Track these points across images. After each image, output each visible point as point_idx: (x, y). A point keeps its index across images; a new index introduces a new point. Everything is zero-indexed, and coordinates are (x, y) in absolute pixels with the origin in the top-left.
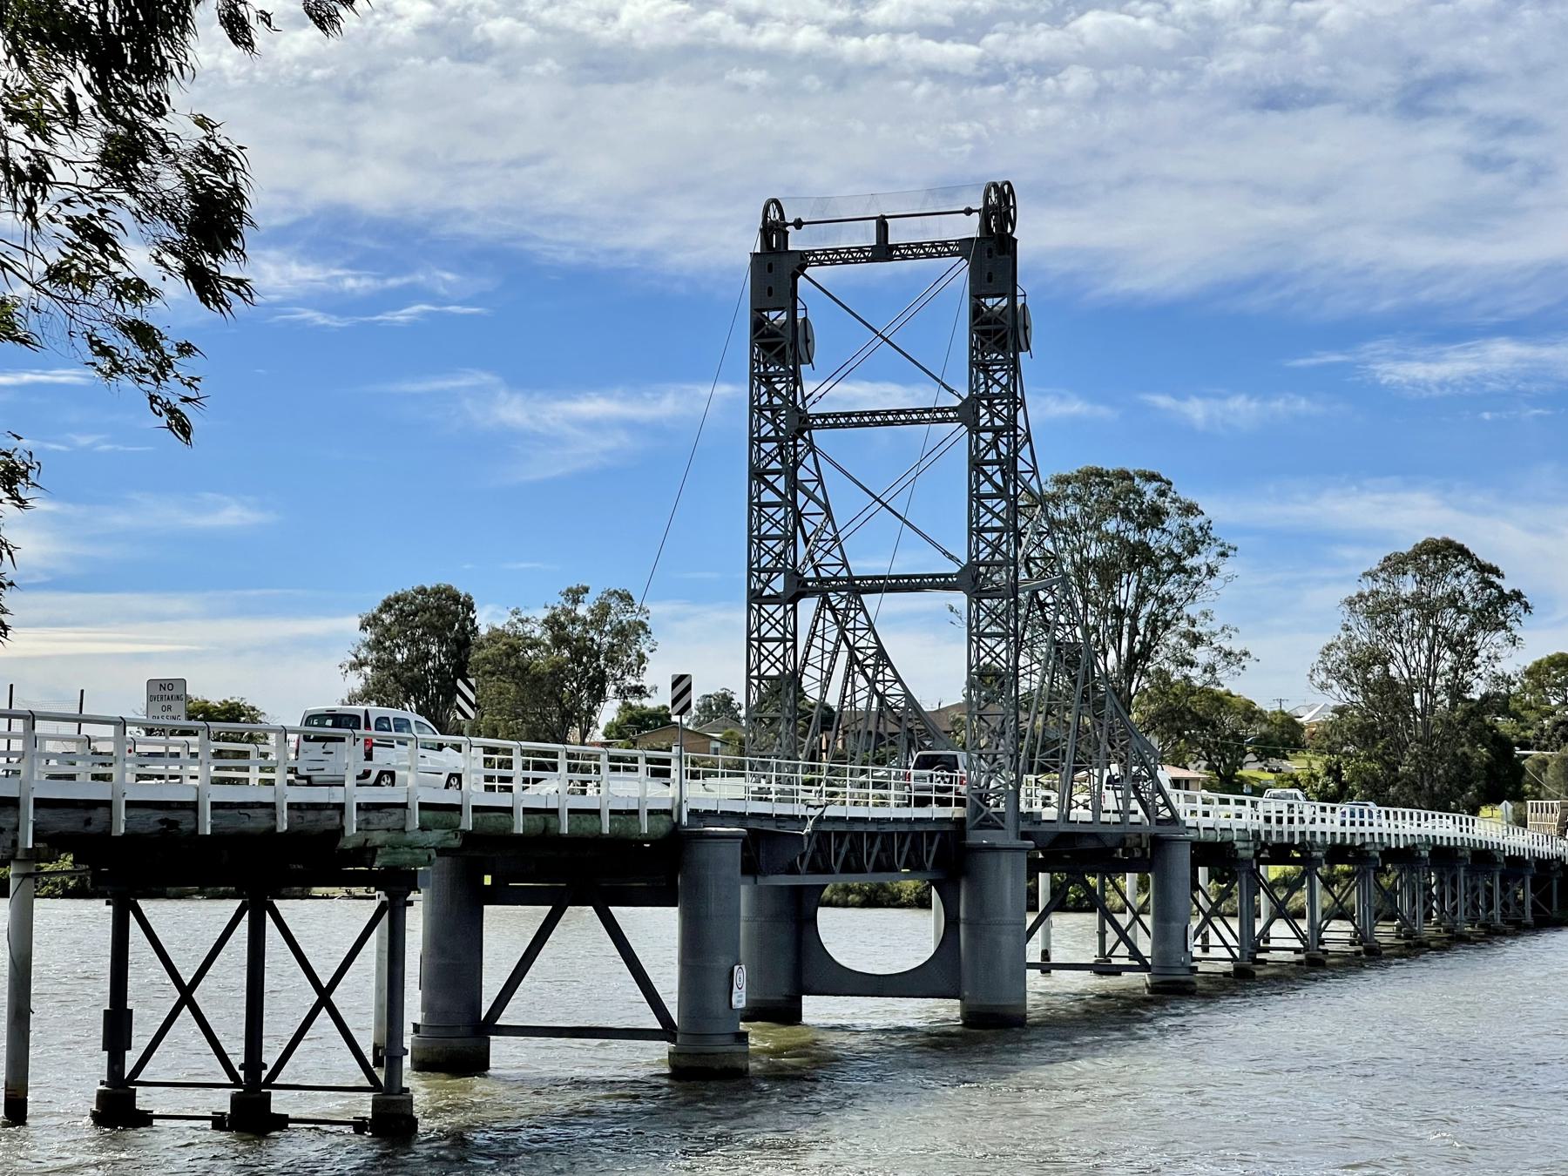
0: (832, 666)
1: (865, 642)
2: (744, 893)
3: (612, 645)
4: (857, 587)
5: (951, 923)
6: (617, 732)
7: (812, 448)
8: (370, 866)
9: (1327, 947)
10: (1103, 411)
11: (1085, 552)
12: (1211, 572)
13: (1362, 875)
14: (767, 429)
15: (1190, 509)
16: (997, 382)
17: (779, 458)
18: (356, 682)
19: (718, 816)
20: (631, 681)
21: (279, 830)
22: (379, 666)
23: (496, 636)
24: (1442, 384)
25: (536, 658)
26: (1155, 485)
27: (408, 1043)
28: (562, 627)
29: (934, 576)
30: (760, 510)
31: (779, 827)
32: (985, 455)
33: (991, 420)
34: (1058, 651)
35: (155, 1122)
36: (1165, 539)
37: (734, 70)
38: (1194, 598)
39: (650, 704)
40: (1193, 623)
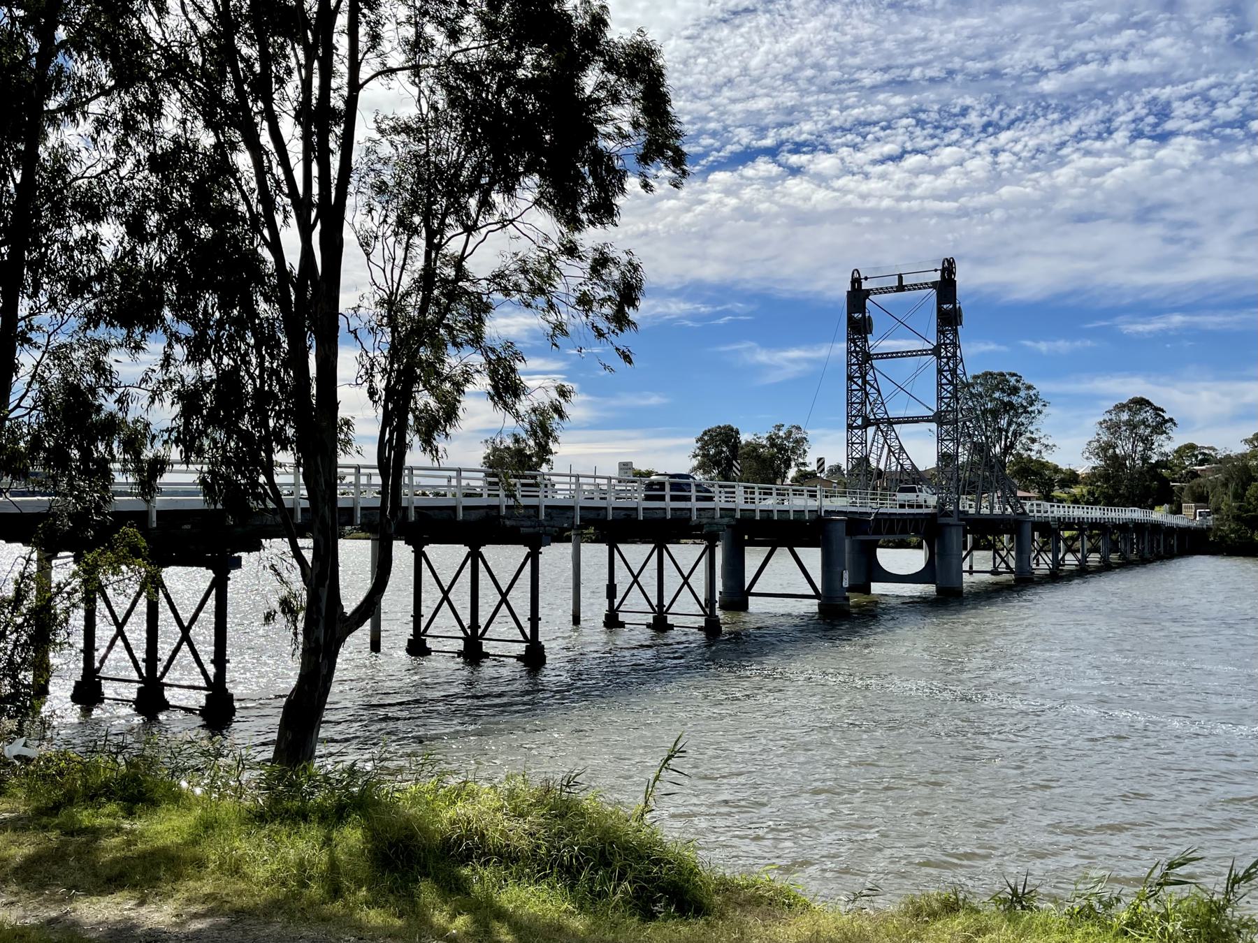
1: (895, 444)
4: (891, 422)
6: (795, 480)
7: (872, 367)
10: (1003, 348)
14: (854, 360)
15: (1029, 388)
18: (695, 462)
20: (801, 460)
22: (704, 456)
23: (748, 444)
24: (1150, 332)
27: (717, 599)
36: (1020, 400)
39: (809, 469)
40: (1032, 433)
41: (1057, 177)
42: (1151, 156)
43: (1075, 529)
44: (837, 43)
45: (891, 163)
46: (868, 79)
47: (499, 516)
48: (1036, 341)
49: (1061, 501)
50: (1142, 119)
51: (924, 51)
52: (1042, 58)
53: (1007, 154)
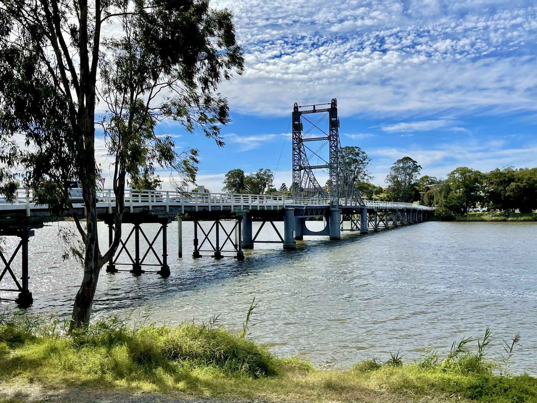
4: (310, 168)
6: (267, 192)
7: (303, 145)
14: (295, 142)
15: (363, 153)
18: (225, 185)
20: (270, 184)
22: (228, 182)
23: (248, 177)
24: (394, 131)
36: (360, 158)
41: (346, 66)
42: (380, 59)
44: (244, 7)
45: (277, 58)
46: (261, 23)
47: (149, 211)
49: (376, 200)
50: (374, 44)
51: (282, 12)
52: (330, 16)
53: (324, 56)
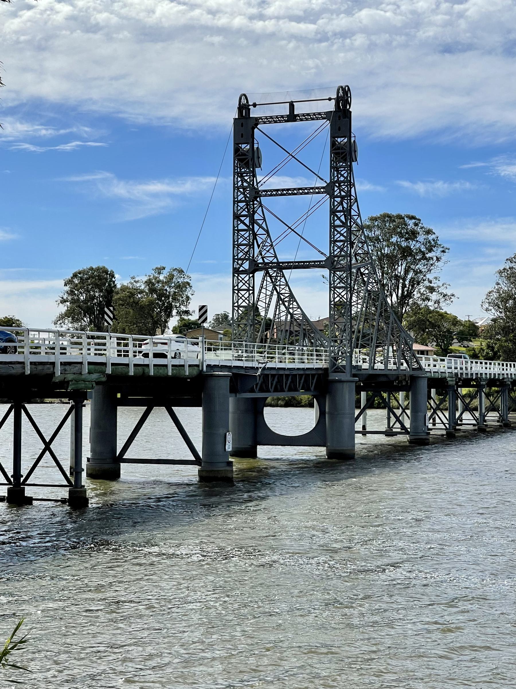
0: (270, 301)
1: (285, 291)
2: (231, 401)
3: (175, 292)
4: (281, 267)
5: (322, 414)
6: (179, 330)
7: (261, 205)
8: (67, 390)
9: (489, 423)
10: (379, 188)
11: (383, 251)
12: (438, 259)
13: (502, 392)
15: (429, 232)
16: (342, 175)
17: (246, 210)
18: (63, 309)
19: (220, 367)
20: (183, 308)
21: (26, 374)
22: (73, 302)
23: (124, 289)
25: (142, 298)
26: (414, 221)
28: (153, 284)
29: (314, 262)
30: (238, 233)
31: (246, 372)
32: (337, 208)
33: (340, 192)
34: (369, 294)
35: (34, 502)
36: (418, 245)
37: (208, 36)
38: (430, 271)
40: (430, 282)
43: (473, 386)
48: (413, 182)
